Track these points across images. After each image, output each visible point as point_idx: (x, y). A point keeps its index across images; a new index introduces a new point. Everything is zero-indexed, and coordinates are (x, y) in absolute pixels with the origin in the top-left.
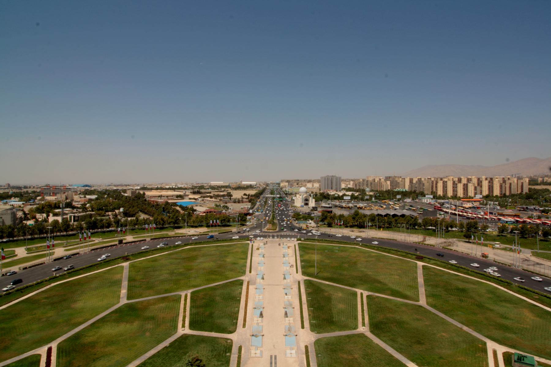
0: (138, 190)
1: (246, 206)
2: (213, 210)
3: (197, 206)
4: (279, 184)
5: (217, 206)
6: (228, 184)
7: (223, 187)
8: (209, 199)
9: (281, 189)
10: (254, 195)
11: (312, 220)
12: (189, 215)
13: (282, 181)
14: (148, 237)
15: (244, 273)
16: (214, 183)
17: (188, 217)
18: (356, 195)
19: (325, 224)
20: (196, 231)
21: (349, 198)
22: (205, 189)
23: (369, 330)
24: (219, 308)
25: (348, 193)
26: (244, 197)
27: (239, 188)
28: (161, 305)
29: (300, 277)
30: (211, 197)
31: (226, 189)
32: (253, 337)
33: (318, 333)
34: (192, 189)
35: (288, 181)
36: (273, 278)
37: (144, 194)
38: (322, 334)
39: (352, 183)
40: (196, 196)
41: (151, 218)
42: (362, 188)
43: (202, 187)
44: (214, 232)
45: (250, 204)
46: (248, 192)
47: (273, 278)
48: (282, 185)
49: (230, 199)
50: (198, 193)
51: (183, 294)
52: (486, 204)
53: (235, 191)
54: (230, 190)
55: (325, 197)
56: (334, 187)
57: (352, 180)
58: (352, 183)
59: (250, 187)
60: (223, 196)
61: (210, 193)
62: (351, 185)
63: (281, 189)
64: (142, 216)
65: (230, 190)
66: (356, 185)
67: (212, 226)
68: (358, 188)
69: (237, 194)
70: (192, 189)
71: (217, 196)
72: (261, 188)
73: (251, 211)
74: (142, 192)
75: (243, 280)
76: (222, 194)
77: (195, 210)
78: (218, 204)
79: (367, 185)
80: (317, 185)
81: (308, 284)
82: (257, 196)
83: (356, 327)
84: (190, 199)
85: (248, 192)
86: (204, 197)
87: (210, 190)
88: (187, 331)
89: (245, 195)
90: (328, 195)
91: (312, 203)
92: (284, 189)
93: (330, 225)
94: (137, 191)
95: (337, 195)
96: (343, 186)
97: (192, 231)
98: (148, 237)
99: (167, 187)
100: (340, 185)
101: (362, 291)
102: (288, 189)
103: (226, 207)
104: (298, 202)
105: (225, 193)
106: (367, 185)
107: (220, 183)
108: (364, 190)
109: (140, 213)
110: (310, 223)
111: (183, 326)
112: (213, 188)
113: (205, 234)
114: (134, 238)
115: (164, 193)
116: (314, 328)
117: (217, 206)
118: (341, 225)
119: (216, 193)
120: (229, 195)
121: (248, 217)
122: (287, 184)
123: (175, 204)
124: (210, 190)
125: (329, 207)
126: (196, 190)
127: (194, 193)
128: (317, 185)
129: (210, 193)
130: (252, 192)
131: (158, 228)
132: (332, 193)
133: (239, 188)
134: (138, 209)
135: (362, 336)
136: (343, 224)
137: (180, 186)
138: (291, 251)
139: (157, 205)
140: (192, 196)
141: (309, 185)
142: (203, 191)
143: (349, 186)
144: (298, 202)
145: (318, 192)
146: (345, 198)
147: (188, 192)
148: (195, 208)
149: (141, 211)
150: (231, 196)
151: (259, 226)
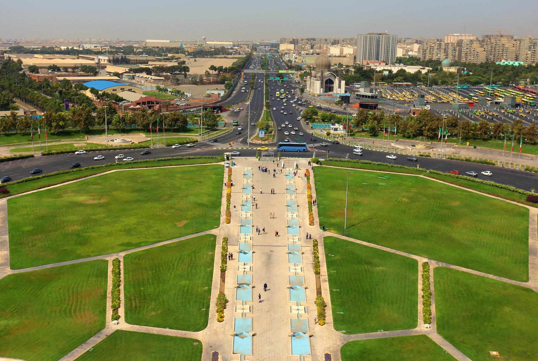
0: (6, 52)
1: (216, 92)
2: (153, 99)
3: (123, 90)
4: (277, 46)
5: (159, 88)
6: (178, 45)
8: (144, 75)
9: (282, 55)
10: (231, 69)
11: (338, 123)
12: (112, 111)
13: (283, 41)
14: (36, 149)
15: (216, 223)
16: (152, 42)
17: (108, 115)
18: (424, 72)
19: (363, 131)
20: (125, 141)
22: (135, 54)
23: (435, 330)
24: (178, 289)
26: (211, 72)
27: (201, 53)
29: (316, 231)
30: (149, 71)
31: (177, 56)
32: (236, 337)
33: (348, 333)
34: (111, 53)
35: (294, 42)
36: (270, 230)
37: (20, 62)
38: (353, 336)
39: (416, 47)
40: (120, 69)
41: (40, 114)
42: (435, 58)
43: (130, 50)
44: (157, 141)
45: (223, 86)
46: (219, 62)
47: (270, 230)
48: (283, 47)
49: (185, 75)
50: (123, 61)
51: (110, 259)
54: (183, 57)
55: (365, 75)
56: (382, 57)
57: (417, 42)
58: (416, 47)
61: (146, 62)
62: (415, 51)
63: (282, 55)
64: (22, 110)
65: (183, 57)
66: (424, 51)
68: (427, 58)
69: (199, 67)
70: (111, 53)
71: (159, 70)
74: (15, 58)
75: (215, 237)
76: (169, 64)
77: (122, 100)
78: (162, 86)
79: (446, 51)
80: (349, 50)
81: (331, 246)
82: (236, 70)
83: (414, 325)
84: (109, 73)
85: (219, 62)
87: (144, 57)
88: (123, 325)
89: (213, 68)
90: (372, 71)
91: (340, 89)
92: (286, 58)
93: (374, 133)
94: (6, 55)
95: (386, 73)
96: (400, 53)
97: (118, 140)
98: (36, 149)
99: (63, 48)
100: (394, 52)
101: (426, 260)
103: (178, 92)
105: (174, 64)
106: (446, 51)
108: (439, 62)
109: (18, 103)
110: (336, 129)
111: (116, 317)
112: (149, 51)
114: (12, 151)
115: (58, 61)
116: (340, 323)
117: (159, 88)
118: (393, 133)
119: (158, 64)
122: (292, 47)
123: (81, 86)
124: (144, 57)
125: (372, 97)
126: (120, 56)
127: (116, 62)
129: (146, 62)
130: (227, 63)
131: (53, 134)
132: (379, 69)
133: (201, 53)
134: (13, 95)
135: (424, 338)
136: (397, 132)
137: (87, 46)
138: (300, 182)
139: (45, 86)
140: (112, 69)
142: (131, 57)
143: (410, 53)
147: (104, 59)
148: (121, 94)
149: (19, 97)
150: (186, 69)
151: (238, 134)
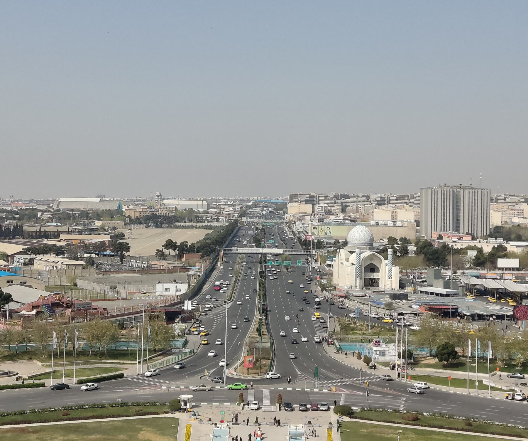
4: (282, 207)
7: (99, 215)
16: (69, 201)
21: (515, 263)
25: (512, 246)
27: (155, 220)
28: (140, 392)
30: (59, 251)
43: (31, 215)
52: (241, 208)
53: (138, 230)
54: (122, 229)
55: (435, 256)
56: (465, 226)
59: (189, 217)
60: (99, 248)
67: (58, 355)
72: (224, 223)
73: (188, 306)
76: (95, 239)
80: (407, 215)
82: (209, 249)
86: (38, 251)
89: (170, 244)
96: (496, 219)
100: (486, 217)
102: (313, 230)
104: (344, 273)
107: (89, 201)
112: (66, 216)
113: (35, 382)
120: (120, 248)
121: (178, 327)
124: (52, 227)
128: (407, 215)
129: (56, 235)
130: (191, 236)
133: (155, 220)
141: (382, 215)
144: (344, 273)
145: (411, 235)
146: (502, 263)
